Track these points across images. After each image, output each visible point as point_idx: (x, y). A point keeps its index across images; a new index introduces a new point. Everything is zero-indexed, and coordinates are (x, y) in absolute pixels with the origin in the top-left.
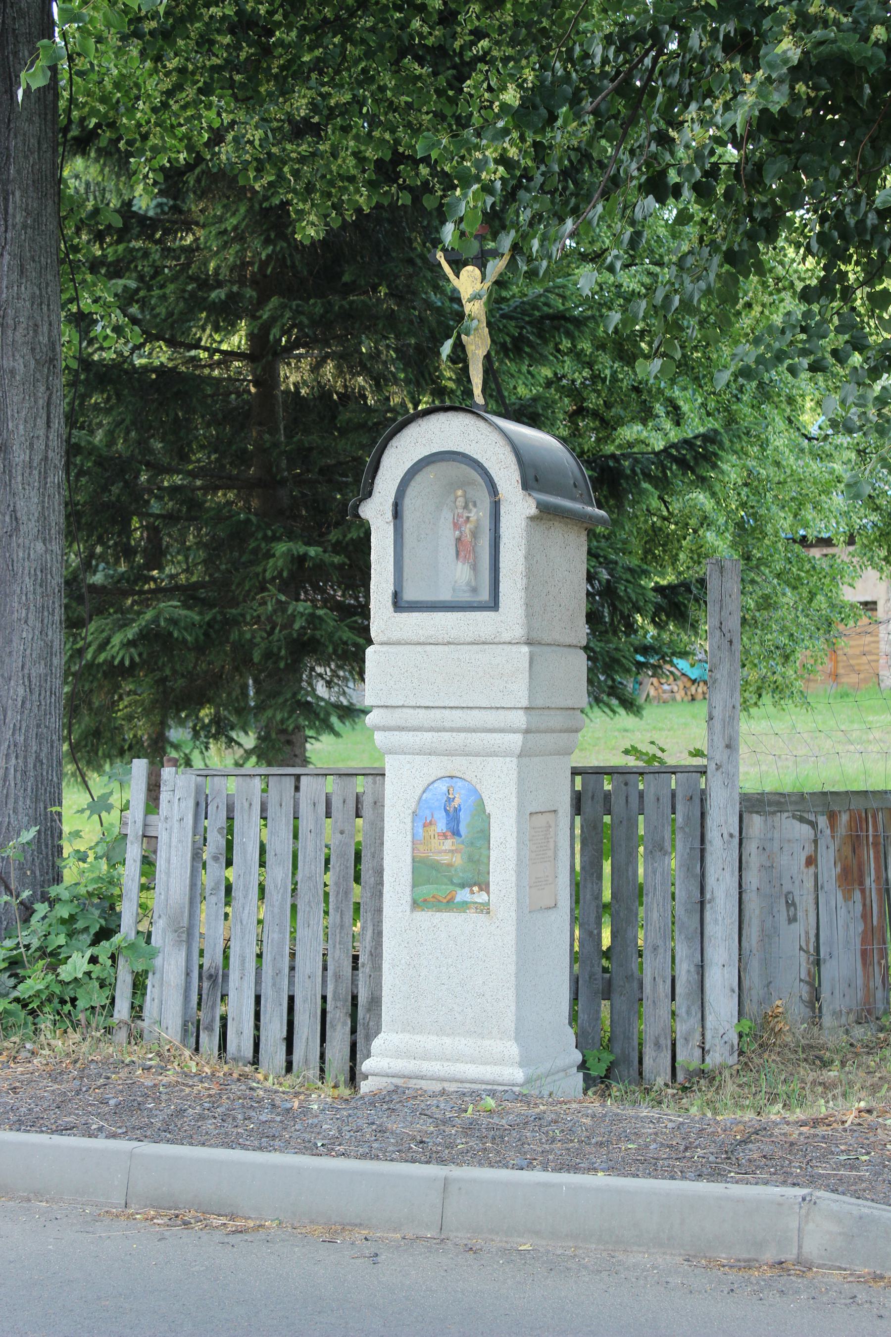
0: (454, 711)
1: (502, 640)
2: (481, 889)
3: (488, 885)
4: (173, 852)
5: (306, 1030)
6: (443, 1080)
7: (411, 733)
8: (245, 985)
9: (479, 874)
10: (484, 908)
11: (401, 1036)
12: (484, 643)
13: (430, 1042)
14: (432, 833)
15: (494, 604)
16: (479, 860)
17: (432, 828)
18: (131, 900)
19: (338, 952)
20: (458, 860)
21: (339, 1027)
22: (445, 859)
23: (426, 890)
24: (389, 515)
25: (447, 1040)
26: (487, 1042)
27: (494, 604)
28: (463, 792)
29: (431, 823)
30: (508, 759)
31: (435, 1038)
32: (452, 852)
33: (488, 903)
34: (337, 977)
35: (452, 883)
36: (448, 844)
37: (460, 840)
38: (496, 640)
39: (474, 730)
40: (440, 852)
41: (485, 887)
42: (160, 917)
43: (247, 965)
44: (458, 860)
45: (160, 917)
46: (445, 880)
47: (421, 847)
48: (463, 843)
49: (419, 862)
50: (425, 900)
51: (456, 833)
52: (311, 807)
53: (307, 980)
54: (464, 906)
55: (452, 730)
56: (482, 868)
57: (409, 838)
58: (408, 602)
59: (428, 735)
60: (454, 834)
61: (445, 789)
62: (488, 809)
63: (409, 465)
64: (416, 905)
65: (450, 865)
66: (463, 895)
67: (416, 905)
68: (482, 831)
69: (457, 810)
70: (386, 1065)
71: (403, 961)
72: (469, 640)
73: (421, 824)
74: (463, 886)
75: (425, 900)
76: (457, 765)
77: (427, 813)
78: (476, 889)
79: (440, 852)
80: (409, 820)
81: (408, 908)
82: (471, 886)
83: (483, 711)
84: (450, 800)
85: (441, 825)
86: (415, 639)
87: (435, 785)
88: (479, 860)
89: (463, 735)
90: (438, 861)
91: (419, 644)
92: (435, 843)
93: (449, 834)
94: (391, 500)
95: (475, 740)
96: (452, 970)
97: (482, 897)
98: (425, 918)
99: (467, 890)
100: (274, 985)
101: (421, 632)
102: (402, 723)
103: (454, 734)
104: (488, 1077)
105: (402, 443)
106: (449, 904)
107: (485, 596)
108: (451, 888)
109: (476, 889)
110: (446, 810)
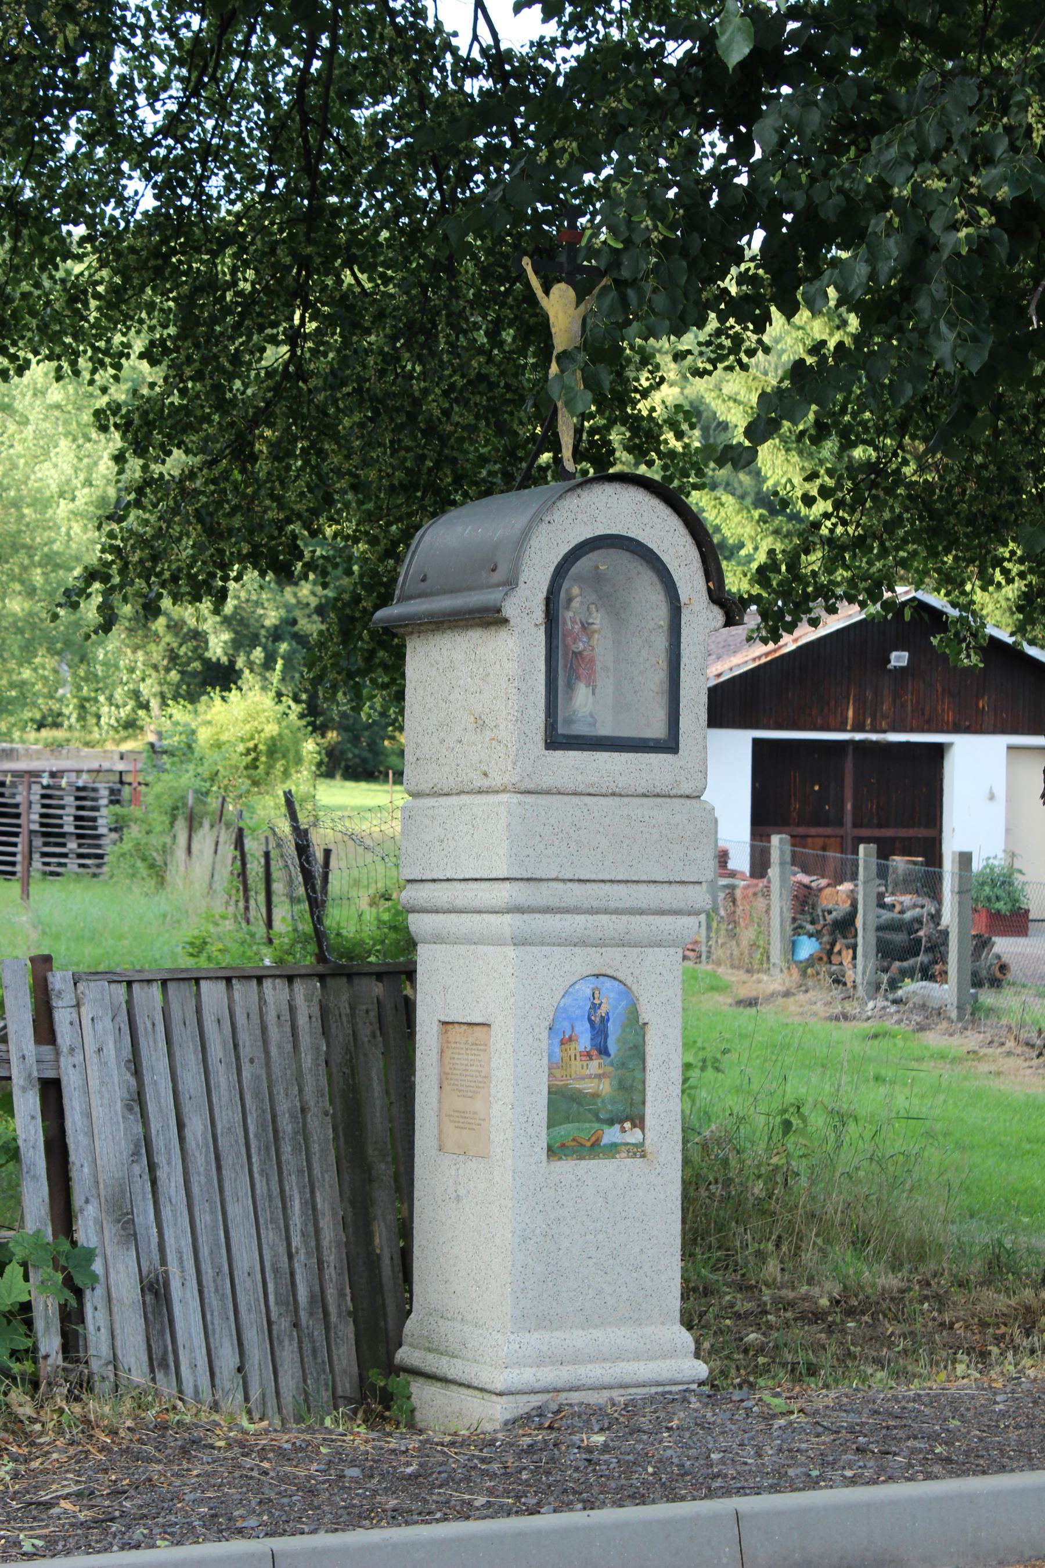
0: (615, 887)
1: (679, 793)
2: (634, 1126)
3: (642, 1119)
4: (95, 1101)
5: (256, 1351)
6: (611, 1387)
7: (558, 916)
8: (189, 1295)
9: (632, 1104)
10: (639, 1151)
11: (536, 1335)
12: (658, 796)
13: (578, 1339)
14: (572, 1053)
15: (555, 741)
16: (632, 1086)
17: (573, 1045)
18: (35, 1178)
19: (271, 1234)
20: (606, 1088)
21: (286, 1343)
22: (589, 1087)
23: (566, 1130)
24: (539, 615)
25: (598, 1333)
26: (648, 1330)
27: (555, 741)
28: (612, 995)
29: (570, 1039)
30: (672, 950)
31: (581, 1332)
32: (599, 1077)
33: (642, 1144)
34: (276, 1271)
35: (599, 1120)
36: (594, 1066)
37: (609, 1060)
38: (672, 793)
39: (641, 912)
40: (583, 1078)
41: (638, 1121)
42: (87, 1201)
43: (186, 1263)
44: (606, 1088)
45: (87, 1201)
46: (590, 1116)
47: (558, 1073)
48: (612, 1064)
49: (556, 1093)
50: (563, 1145)
51: (604, 1051)
52: (215, 1025)
53: (247, 1279)
54: (613, 1149)
55: (617, 912)
56: (636, 1097)
57: (545, 1061)
58: (564, 736)
59: (580, 919)
60: (600, 1052)
61: (589, 992)
62: (644, 1017)
63: (565, 549)
64: (554, 1152)
65: (595, 1095)
66: (612, 1135)
67: (554, 1152)
68: (635, 1047)
69: (605, 1020)
70: (532, 1379)
71: (538, 1231)
72: (640, 791)
73: (557, 1041)
74: (611, 1122)
75: (563, 1145)
76: (610, 959)
77: (566, 1025)
78: (627, 1125)
79: (583, 1078)
80: (545, 1035)
81: (544, 1157)
82: (621, 1122)
83: (659, 887)
84: (595, 1007)
85: (584, 1041)
86: (571, 786)
87: (577, 987)
88: (632, 1086)
89: (625, 918)
90: (580, 1091)
91: (575, 794)
92: (576, 1066)
93: (595, 1053)
94: (542, 595)
95: (640, 925)
96: (601, 1237)
97: (634, 1136)
98: (567, 1168)
99: (617, 1127)
100: (217, 1290)
101: (580, 778)
102: (554, 902)
103: (614, 917)
104: (665, 1376)
105: (556, 517)
106: (594, 1149)
107: (657, 730)
108: (596, 1125)
109: (627, 1125)
110: (590, 1020)
